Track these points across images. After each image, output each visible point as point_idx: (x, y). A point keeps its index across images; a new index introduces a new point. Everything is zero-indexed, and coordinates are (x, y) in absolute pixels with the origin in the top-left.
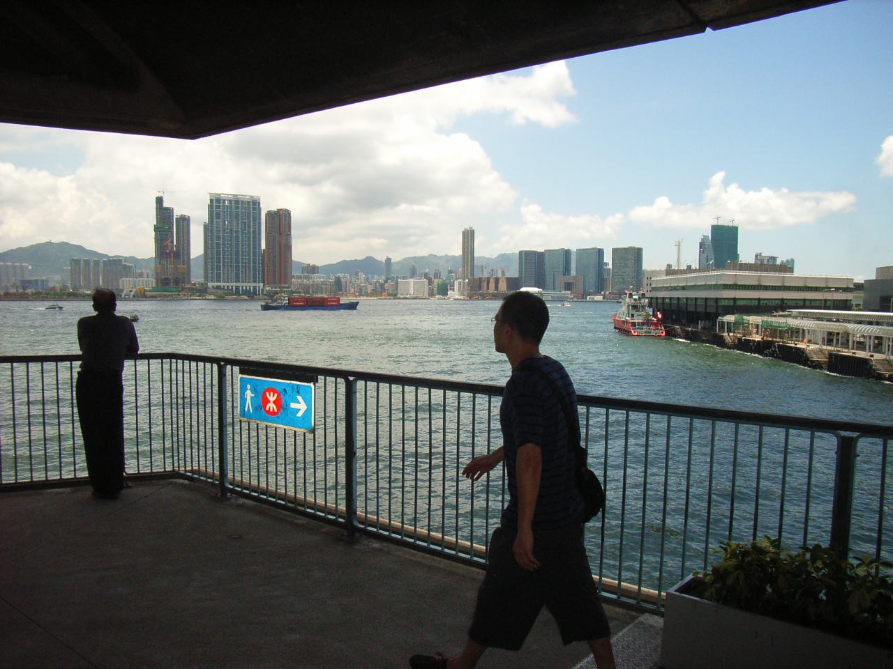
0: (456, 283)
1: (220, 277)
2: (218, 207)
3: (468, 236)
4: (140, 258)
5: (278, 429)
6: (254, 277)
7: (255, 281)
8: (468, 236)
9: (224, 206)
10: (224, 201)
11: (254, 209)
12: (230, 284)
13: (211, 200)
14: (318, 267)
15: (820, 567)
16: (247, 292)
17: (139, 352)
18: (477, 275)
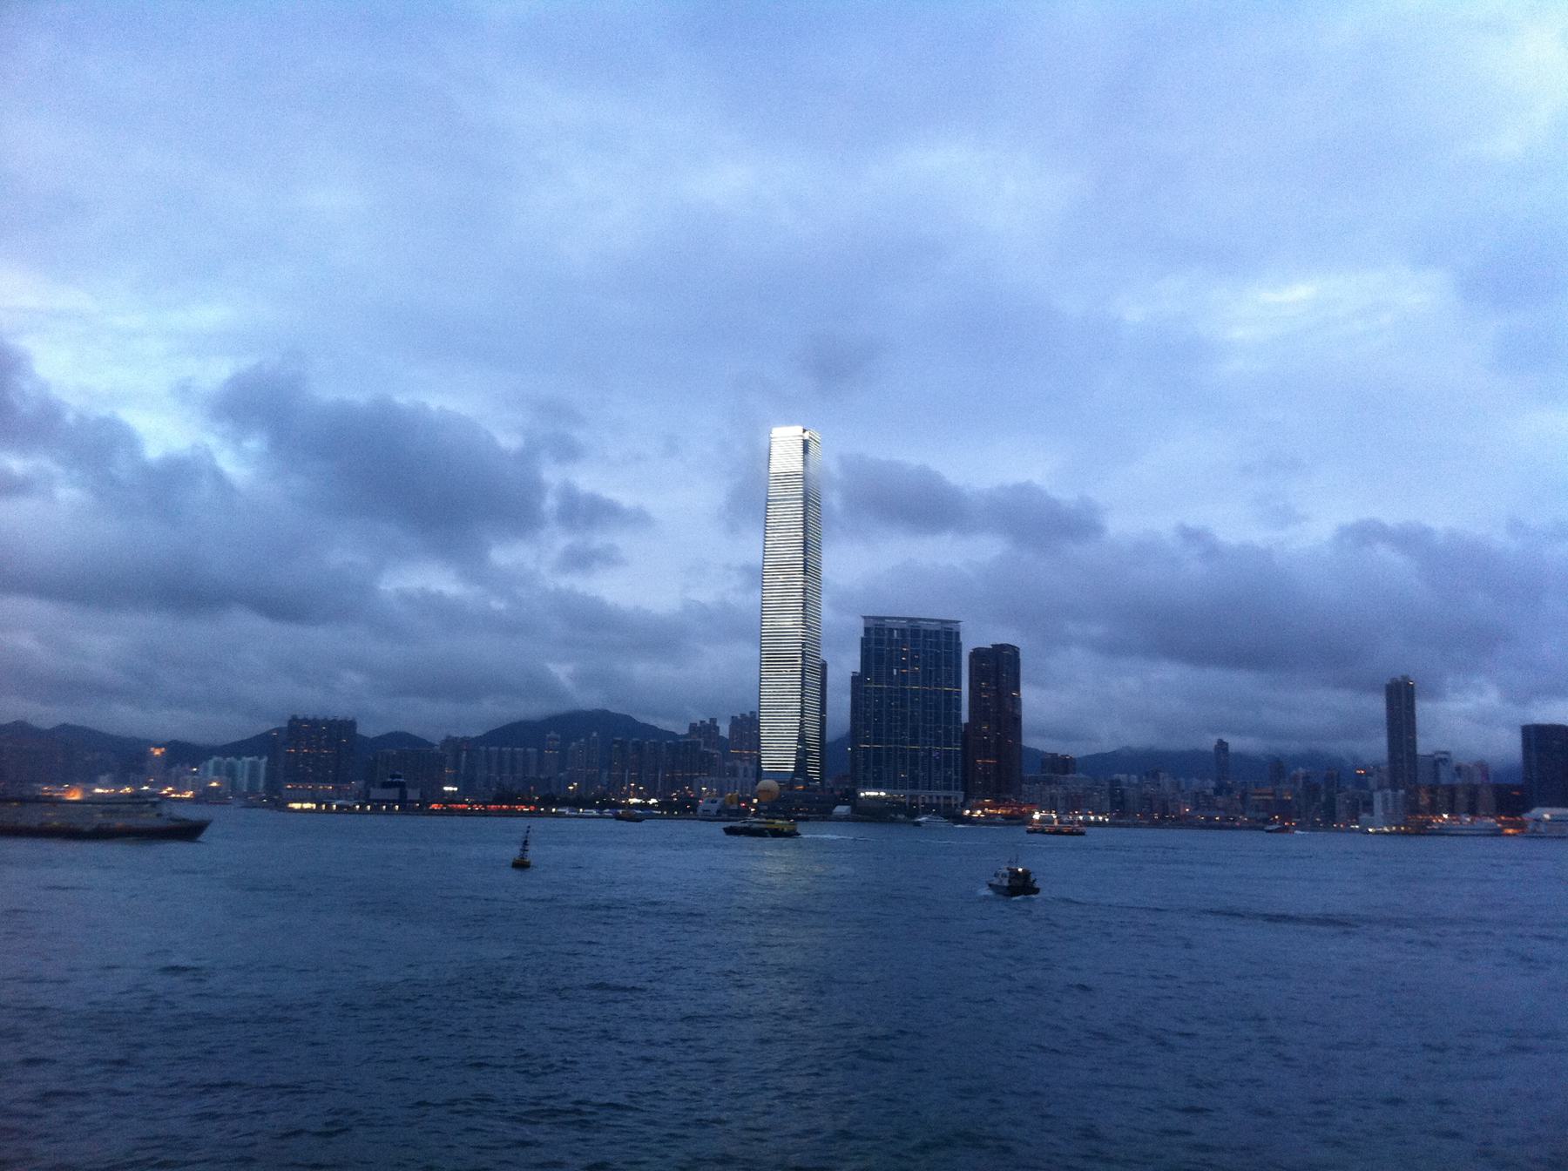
0: (1378, 797)
2: (879, 642)
3: (1401, 699)
7: (948, 788)
9: (891, 641)
10: (891, 630)
11: (948, 645)
12: (935, 793)
13: (867, 630)
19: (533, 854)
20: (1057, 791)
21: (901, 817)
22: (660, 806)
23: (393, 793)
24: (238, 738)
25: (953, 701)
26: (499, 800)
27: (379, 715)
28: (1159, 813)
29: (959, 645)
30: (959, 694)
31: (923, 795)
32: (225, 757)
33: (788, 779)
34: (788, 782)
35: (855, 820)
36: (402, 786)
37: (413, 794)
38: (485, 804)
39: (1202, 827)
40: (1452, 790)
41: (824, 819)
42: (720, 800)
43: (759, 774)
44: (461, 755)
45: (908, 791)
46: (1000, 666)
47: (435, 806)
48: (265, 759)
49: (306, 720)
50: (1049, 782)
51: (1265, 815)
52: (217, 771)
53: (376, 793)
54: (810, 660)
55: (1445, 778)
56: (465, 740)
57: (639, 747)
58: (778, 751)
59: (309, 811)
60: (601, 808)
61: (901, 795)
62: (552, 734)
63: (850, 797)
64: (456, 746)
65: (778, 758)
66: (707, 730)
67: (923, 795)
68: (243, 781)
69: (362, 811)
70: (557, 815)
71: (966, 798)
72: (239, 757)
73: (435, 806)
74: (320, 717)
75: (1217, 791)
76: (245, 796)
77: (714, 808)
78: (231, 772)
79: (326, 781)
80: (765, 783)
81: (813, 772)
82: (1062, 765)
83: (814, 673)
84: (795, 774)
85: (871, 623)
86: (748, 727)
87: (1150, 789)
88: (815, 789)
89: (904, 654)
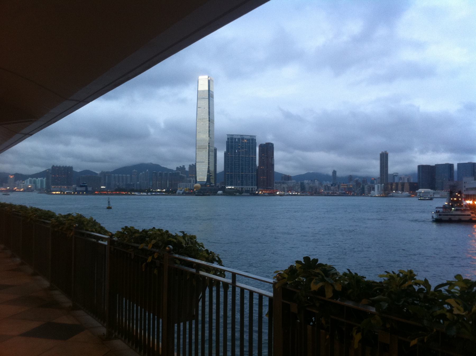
0: (376, 186)
1: (243, 183)
2: (232, 142)
3: (384, 158)
4: (434, 165)
5: (238, 277)
6: (252, 183)
7: (252, 185)
8: (384, 158)
9: (235, 142)
10: (235, 139)
11: (252, 143)
12: (248, 187)
13: (228, 139)
14: (291, 177)
15: (180, 250)
16: (247, 191)
17: (416, 290)
18: (390, 181)
19: (112, 204)
20: (285, 186)
21: (238, 194)
22: (165, 192)
23: (84, 189)
24: (35, 173)
25: (254, 159)
26: (116, 190)
27: (79, 166)
28: (315, 192)
29: (256, 143)
30: (256, 158)
31: (245, 187)
32: (33, 178)
33: (205, 183)
34: (203, 185)
35: (224, 195)
36: (86, 186)
37: (90, 189)
38: (112, 191)
39: (325, 195)
40: (397, 184)
41: (215, 195)
42: (183, 190)
43: (196, 182)
44: (106, 177)
45: (241, 187)
46: (268, 149)
47: (96, 192)
48: (45, 179)
49: (57, 167)
50: (283, 183)
51: (344, 192)
52: (30, 183)
53: (78, 189)
54: (211, 148)
55: (396, 180)
56: (107, 172)
57: (161, 174)
58: (202, 176)
59: (58, 194)
60: (147, 192)
61: (239, 187)
62: (134, 170)
63: (223, 189)
64: (104, 174)
65: (201, 177)
66: (182, 169)
67: (245, 187)
68: (39, 186)
69: (74, 194)
70: (134, 195)
71: (258, 188)
72: (37, 178)
73: (96, 192)
74: (61, 166)
75: (332, 185)
76: (40, 190)
77: (181, 192)
78: (35, 182)
79: (64, 185)
80: (198, 185)
81: (212, 181)
82: (287, 178)
83: (213, 153)
84: (207, 182)
85: (229, 137)
86: (193, 168)
87: (311, 185)
88: (213, 186)
89: (239, 146)
